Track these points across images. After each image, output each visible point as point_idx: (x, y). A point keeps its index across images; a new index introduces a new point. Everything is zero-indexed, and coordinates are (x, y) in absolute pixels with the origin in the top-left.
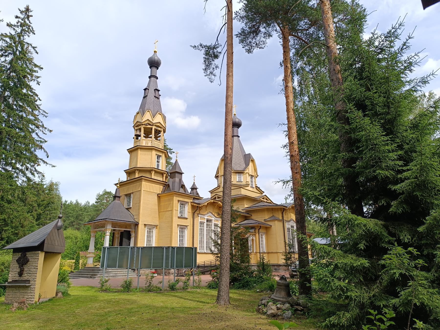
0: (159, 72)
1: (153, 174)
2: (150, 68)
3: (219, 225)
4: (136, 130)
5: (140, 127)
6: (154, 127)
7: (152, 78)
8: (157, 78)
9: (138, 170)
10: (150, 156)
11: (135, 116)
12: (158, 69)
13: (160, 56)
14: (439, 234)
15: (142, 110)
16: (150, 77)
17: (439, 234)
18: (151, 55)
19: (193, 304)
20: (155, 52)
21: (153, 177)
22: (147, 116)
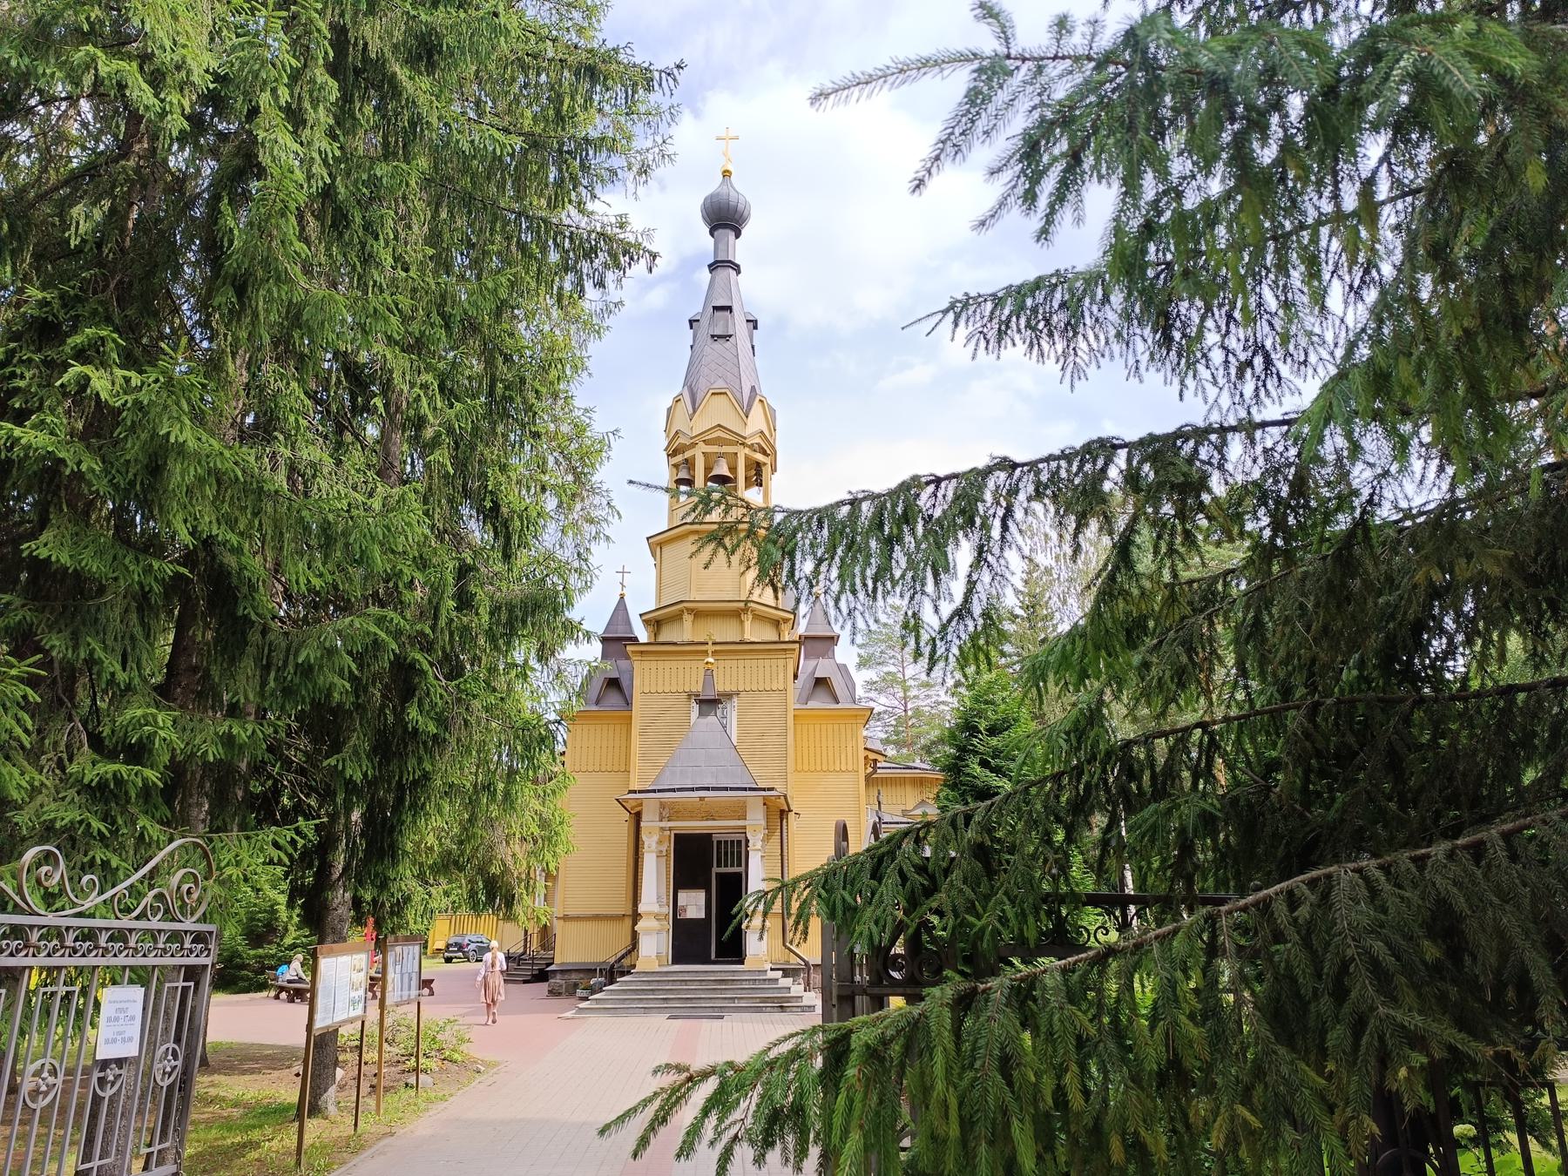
0: (741, 249)
1: (747, 624)
2: (712, 234)
3: (291, 1142)
4: (676, 466)
5: (688, 454)
6: (743, 452)
7: (722, 273)
8: (737, 269)
9: (690, 611)
10: (305, 1008)
11: (669, 410)
12: (737, 236)
13: (746, 190)
14: (1276, 1171)
15: (693, 396)
16: (713, 267)
17: (1276, 1171)
18: (712, 185)
19: (855, 1137)
20: (726, 174)
21: (748, 637)
22: (717, 413)
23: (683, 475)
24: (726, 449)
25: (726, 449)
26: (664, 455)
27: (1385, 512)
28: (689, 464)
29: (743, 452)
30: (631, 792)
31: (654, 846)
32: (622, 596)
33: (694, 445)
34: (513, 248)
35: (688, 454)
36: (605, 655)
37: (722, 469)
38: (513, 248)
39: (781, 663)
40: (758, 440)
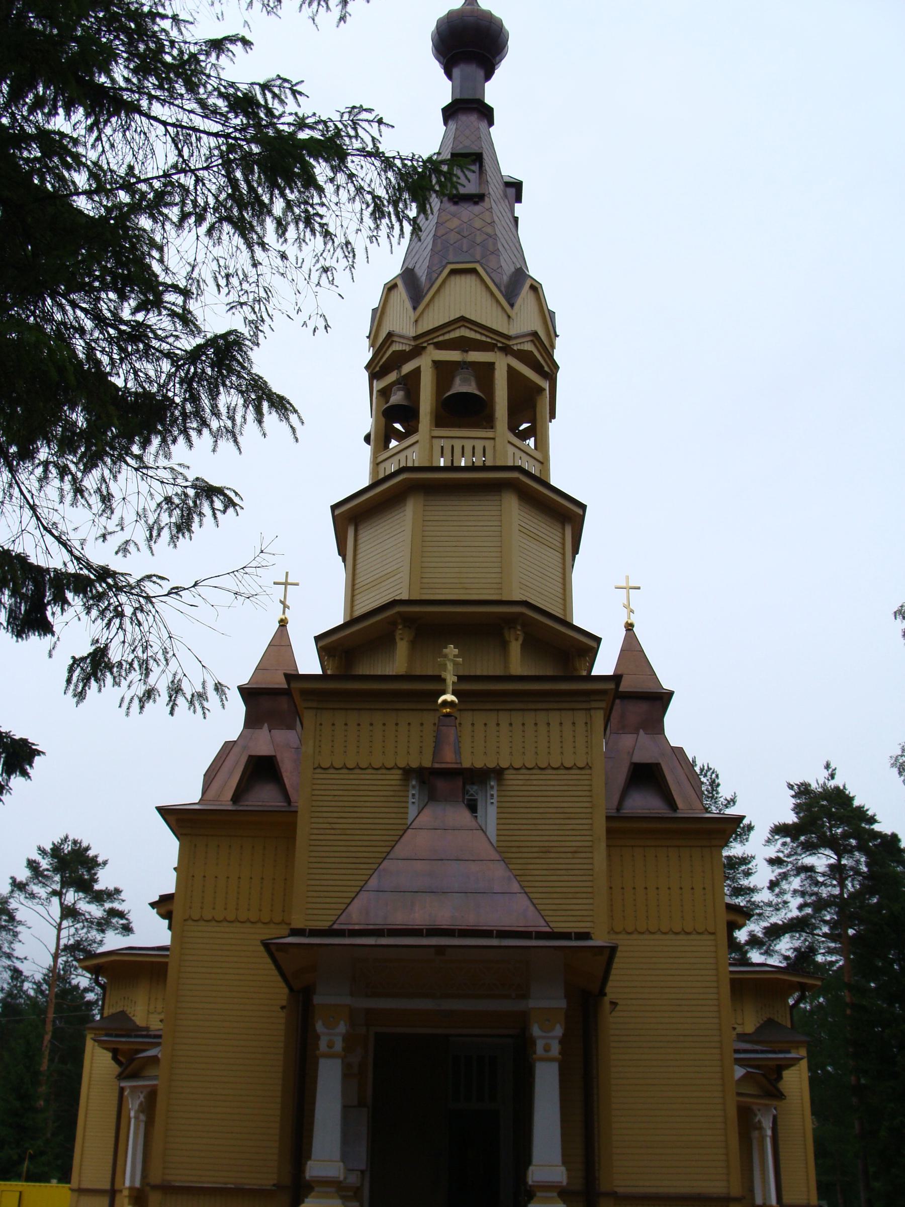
1: (515, 648)
5: (407, 368)
23: (397, 398)
24: (475, 356)
25: (475, 356)
26: (365, 375)
27: (116, 117)
28: (411, 383)
29: (502, 363)
30: (295, 932)
31: (339, 1046)
32: (283, 623)
33: (417, 351)
34: (789, 860)
35: (407, 368)
36: (251, 721)
37: (463, 386)
38: (789, 860)
39: (581, 717)
40: (528, 347)
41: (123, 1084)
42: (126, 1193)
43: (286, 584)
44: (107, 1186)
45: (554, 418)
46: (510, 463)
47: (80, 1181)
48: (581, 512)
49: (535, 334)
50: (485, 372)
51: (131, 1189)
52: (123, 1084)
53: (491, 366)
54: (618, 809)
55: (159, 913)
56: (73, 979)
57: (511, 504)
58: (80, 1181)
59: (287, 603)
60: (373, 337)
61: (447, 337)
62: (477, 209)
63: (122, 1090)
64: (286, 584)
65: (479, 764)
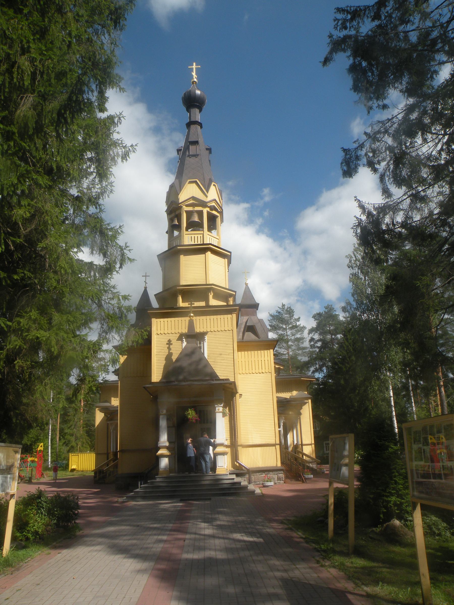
41: (108, 422)
42: (112, 453)
43: (146, 276)
44: (106, 452)
45: (223, 222)
46: (208, 243)
47: (276, 449)
48: (230, 254)
49: (215, 200)
50: (200, 213)
51: (113, 452)
52: (108, 422)
53: (202, 212)
54: (243, 339)
55: (115, 374)
56: (27, 336)
57: (209, 253)
58: (276, 449)
59: (147, 282)
60: (167, 202)
61: (189, 203)
62: (197, 159)
63: (108, 424)
64: (146, 276)
65: (202, 331)
